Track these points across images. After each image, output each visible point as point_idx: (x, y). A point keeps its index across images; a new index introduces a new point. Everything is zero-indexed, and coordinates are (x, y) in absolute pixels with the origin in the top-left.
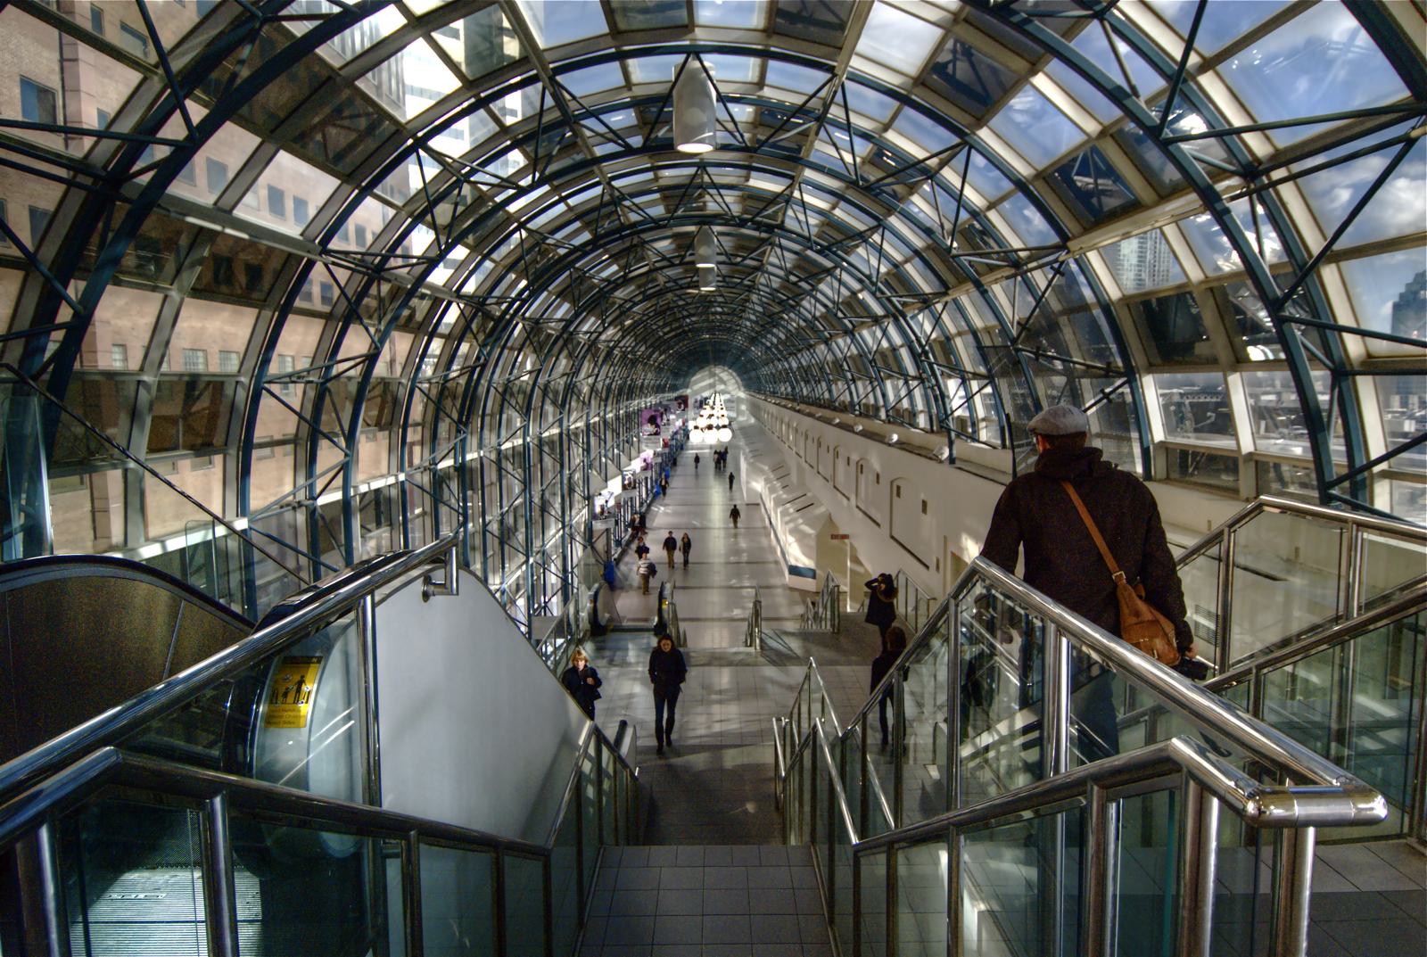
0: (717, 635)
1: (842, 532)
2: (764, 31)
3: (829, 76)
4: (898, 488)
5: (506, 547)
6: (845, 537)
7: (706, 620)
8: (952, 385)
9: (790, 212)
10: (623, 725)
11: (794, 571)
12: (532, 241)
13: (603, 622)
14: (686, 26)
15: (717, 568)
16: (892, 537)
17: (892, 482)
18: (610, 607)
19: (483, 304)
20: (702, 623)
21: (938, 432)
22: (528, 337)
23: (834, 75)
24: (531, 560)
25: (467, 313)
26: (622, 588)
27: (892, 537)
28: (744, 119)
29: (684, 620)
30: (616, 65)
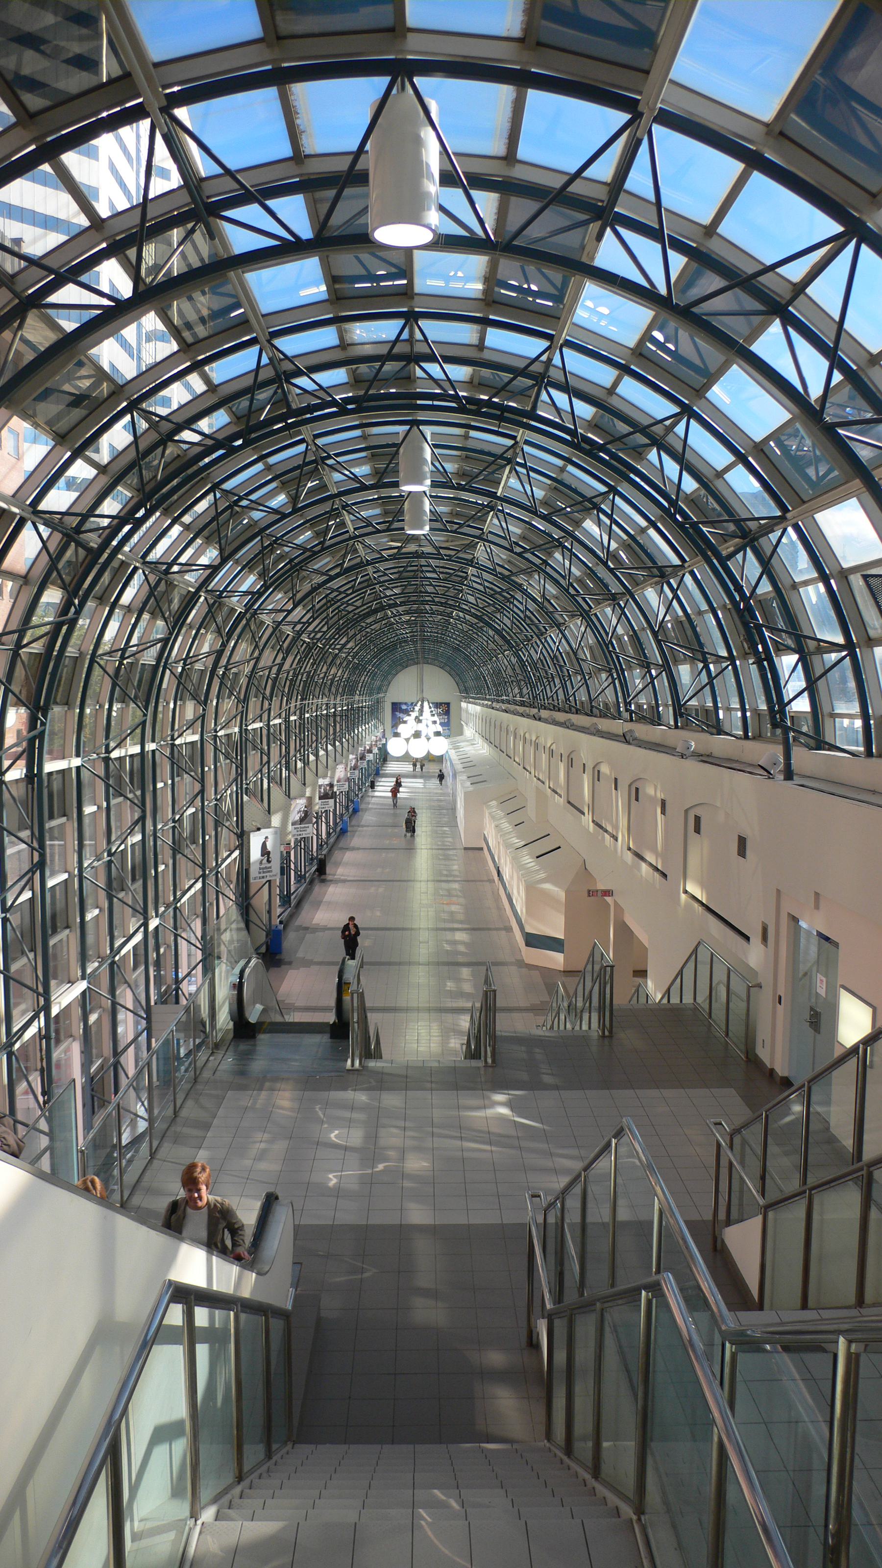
0: (423, 1032)
1: (601, 886)
2: (520, 40)
3: (625, 117)
4: (698, 819)
5: (179, 856)
6: (607, 893)
7: (407, 1010)
8: (787, 661)
9: (544, 396)
10: (270, 1201)
11: (534, 941)
12: (154, 437)
13: (253, 1018)
14: (391, 30)
15: (424, 936)
16: (569, 802)
17: (686, 811)
18: (266, 991)
19: (167, 572)
20: (403, 1015)
21: (682, 728)
22: (209, 611)
23: (516, 443)
24: (153, 923)
25: (52, 546)
26: (290, 963)
27: (569, 802)
28: (452, 471)
29: (518, 108)
30: (271, 93)
